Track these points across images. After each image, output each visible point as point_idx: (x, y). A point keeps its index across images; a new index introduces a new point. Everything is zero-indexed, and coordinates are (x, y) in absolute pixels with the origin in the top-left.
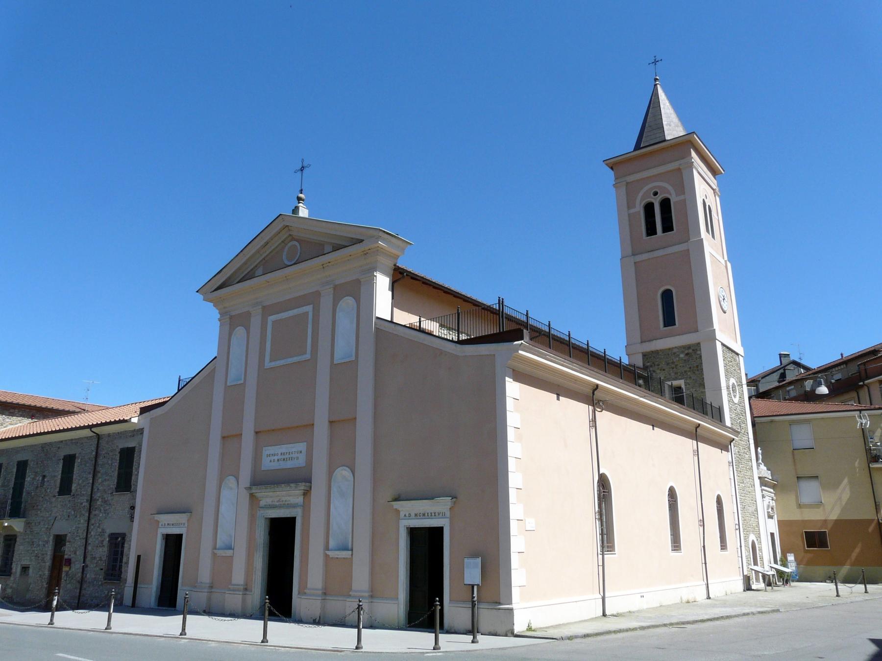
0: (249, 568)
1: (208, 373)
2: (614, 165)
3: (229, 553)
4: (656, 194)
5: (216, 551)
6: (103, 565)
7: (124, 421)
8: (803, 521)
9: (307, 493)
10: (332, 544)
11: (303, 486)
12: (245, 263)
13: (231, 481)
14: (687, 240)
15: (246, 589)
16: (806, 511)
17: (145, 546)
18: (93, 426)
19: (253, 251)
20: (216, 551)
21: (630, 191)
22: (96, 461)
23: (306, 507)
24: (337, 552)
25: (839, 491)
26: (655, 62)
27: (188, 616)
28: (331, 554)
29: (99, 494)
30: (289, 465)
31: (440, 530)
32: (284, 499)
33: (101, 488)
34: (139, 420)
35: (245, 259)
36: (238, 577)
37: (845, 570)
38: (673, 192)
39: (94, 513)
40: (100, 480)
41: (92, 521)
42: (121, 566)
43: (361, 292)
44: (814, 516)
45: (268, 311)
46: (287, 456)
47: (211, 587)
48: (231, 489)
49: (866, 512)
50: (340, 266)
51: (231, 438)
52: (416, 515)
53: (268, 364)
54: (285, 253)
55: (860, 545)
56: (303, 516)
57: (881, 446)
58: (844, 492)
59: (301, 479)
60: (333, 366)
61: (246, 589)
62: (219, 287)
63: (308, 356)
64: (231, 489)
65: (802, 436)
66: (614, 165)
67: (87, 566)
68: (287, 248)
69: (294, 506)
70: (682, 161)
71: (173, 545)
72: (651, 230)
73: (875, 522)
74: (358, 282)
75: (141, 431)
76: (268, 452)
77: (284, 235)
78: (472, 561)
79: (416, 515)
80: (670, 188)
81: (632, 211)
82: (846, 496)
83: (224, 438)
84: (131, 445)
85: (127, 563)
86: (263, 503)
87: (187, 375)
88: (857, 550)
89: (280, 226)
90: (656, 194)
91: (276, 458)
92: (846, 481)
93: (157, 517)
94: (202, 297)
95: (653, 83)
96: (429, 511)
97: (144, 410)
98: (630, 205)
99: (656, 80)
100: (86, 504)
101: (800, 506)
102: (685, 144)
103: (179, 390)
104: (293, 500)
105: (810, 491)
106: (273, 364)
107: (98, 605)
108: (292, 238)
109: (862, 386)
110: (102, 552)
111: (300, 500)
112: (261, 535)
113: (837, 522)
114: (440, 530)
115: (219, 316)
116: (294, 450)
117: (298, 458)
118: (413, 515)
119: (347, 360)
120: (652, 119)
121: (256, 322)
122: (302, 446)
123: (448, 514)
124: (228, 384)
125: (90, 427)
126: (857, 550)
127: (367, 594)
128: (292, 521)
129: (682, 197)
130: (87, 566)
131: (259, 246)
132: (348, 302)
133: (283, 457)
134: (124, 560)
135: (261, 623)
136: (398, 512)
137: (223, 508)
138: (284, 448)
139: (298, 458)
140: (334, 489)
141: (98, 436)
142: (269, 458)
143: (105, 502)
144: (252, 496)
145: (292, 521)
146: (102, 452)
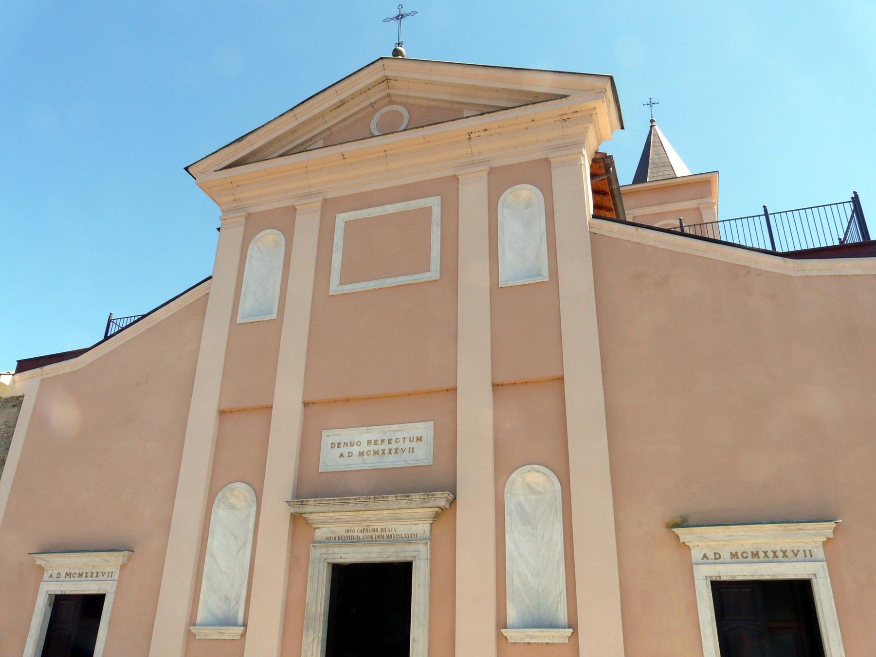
1: (194, 300)
3: (234, 632)
9: (445, 515)
10: (512, 614)
11: (441, 500)
12: (293, 131)
13: (239, 494)
26: (651, 104)
30: (390, 462)
32: (379, 526)
34: (13, 382)
35: (294, 124)
45: (330, 207)
46: (385, 446)
48: (233, 507)
50: (506, 139)
51: (247, 413)
52: (734, 555)
53: (335, 287)
59: (435, 485)
60: (495, 290)
63: (434, 274)
64: (233, 507)
68: (378, 115)
69: (410, 539)
75: (17, 402)
77: (377, 94)
83: (222, 413)
87: (125, 311)
89: (379, 76)
95: (650, 124)
97: (24, 366)
99: (652, 121)
103: (107, 338)
104: (402, 529)
106: (349, 288)
108: (390, 99)
111: (423, 528)
115: (220, 214)
116: (400, 435)
117: (411, 450)
119: (531, 281)
121: (307, 226)
122: (424, 429)
123: (820, 553)
124: (239, 321)
131: (327, 105)
133: (373, 448)
137: (215, 543)
138: (375, 433)
142: (337, 451)
144: (296, 519)
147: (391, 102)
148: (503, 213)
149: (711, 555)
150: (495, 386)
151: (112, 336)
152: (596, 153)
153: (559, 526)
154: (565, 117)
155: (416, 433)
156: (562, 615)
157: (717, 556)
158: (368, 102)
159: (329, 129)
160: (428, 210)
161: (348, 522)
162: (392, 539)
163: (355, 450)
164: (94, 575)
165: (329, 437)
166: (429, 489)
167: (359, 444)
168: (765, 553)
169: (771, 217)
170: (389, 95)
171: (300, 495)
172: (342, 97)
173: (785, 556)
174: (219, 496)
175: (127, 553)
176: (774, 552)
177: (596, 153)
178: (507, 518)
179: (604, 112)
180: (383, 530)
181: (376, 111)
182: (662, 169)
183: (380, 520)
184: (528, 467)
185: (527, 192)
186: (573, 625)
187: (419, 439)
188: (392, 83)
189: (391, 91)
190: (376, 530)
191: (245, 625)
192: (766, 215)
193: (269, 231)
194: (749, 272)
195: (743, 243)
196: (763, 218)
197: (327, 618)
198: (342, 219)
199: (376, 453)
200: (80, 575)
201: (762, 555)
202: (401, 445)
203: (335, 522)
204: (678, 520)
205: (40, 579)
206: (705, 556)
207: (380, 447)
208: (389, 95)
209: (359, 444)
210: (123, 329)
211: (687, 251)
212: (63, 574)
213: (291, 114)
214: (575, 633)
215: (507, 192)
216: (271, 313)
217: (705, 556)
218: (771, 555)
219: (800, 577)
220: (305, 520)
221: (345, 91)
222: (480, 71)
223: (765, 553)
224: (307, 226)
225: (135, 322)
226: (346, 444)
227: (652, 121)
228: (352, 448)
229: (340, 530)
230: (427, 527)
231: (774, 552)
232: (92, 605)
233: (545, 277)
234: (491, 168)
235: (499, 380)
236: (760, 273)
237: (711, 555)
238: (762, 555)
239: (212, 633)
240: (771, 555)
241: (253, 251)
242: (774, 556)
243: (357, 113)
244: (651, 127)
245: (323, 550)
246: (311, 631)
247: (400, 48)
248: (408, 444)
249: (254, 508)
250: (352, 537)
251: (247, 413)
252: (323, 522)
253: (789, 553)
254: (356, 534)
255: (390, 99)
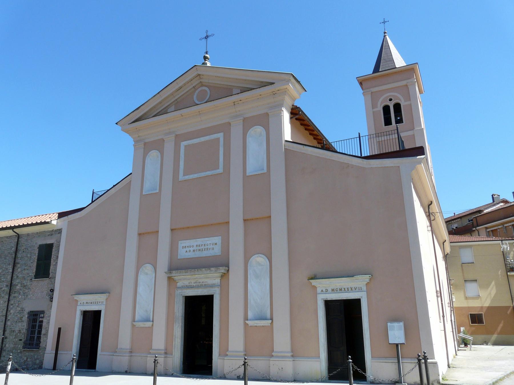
0: (168, 336)
1: (124, 186)
2: (362, 82)
3: (149, 324)
4: (391, 100)
5: (134, 323)
6: (23, 337)
7: (45, 223)
8: (468, 307)
9: (225, 276)
10: (250, 315)
11: (222, 270)
12: (160, 103)
13: (148, 268)
14: (413, 129)
15: (166, 353)
16: (470, 301)
17: (63, 320)
18: (15, 227)
19: (169, 93)
20: (134, 323)
21: (374, 98)
22: (16, 254)
23: (224, 286)
24: (256, 322)
25: (490, 289)
26: (384, 22)
27: (158, 378)
28: (250, 323)
29: (18, 281)
30: (204, 254)
31: (357, 302)
32: (201, 281)
33: (20, 276)
34: (57, 223)
36: (159, 342)
37: (494, 337)
38: (402, 99)
39: (13, 295)
40: (19, 270)
41: (12, 302)
42: (39, 338)
43: (267, 121)
44: (476, 304)
45: (179, 138)
46: (203, 247)
47: (131, 352)
48: (147, 274)
49: (506, 302)
50: (251, 103)
51: (148, 235)
52: (333, 290)
53: (181, 177)
54: (196, 94)
55: (502, 322)
56: (221, 294)
57: (513, 262)
58: (492, 290)
59: (221, 264)
60: (246, 178)
61: (167, 353)
62: (138, 119)
63: (220, 170)
64: (147, 274)
65: (467, 256)
66: (362, 82)
67: (6, 338)
68: (197, 92)
69: (212, 286)
70: (409, 80)
71: (92, 321)
72: (388, 122)
73: (511, 308)
74: (267, 115)
75: (59, 231)
76: (184, 245)
77: (195, 83)
78: (396, 324)
79: (333, 290)
80: (400, 96)
81: (375, 110)
82: (494, 292)
84: (49, 242)
85: (46, 335)
86: (179, 284)
88: (501, 325)
89: (195, 74)
90: (391, 100)
91: (192, 249)
92: (493, 283)
93: (77, 297)
94: (120, 128)
95: (383, 35)
96: (353, 287)
97: (61, 215)
98: (374, 106)
99: (385, 33)
100: (7, 289)
101: (466, 298)
102: (409, 71)
103: (93, 202)
104: (210, 282)
105: (472, 289)
106: (187, 177)
107: (35, 369)
108: (202, 84)
109: (474, 230)
110: (23, 326)
111: (217, 281)
112: (179, 309)
113: (489, 308)
114: (357, 302)
116: (208, 242)
117: (213, 249)
118: (330, 290)
119: (260, 172)
120: (382, 56)
121: (169, 147)
122: (217, 240)
123: (364, 288)
125: (11, 228)
126: (501, 325)
127: (289, 354)
128: (209, 300)
129: (408, 103)
130: (6, 338)
132: (258, 130)
133: (198, 248)
134: (43, 332)
135: (152, 378)
136: (315, 288)
137: (140, 289)
138: (199, 241)
139: (213, 249)
140: (250, 272)
141: (18, 236)
142: (185, 250)
143: (25, 286)
144: (170, 279)
145: (209, 300)
146: (21, 248)
147: (202, 85)
148: (249, 139)
149: (324, 290)
150: (245, 220)
151: (95, 201)
152: (293, 105)
153: (268, 280)
154: (274, 93)
155: (214, 242)
156: (269, 316)
157: (327, 290)
158: (192, 87)
159: (176, 100)
160: (218, 139)
161: (189, 279)
162: (206, 286)
163: (192, 249)
164: (96, 303)
165: (182, 244)
166: (217, 266)
167: (193, 246)
168: (344, 289)
169: (361, 138)
170: (201, 82)
171: (171, 269)
172: (180, 85)
173: (352, 290)
174: (141, 270)
175: (107, 294)
176: (348, 288)
177: (293, 105)
178: (249, 276)
179: (292, 87)
180: (203, 282)
181: (196, 90)
182: (388, 63)
183: (200, 278)
184: (257, 255)
185: (259, 129)
186: (272, 319)
187: (216, 244)
188: (201, 77)
189: (201, 80)
190: (200, 282)
191: (153, 321)
192: (359, 137)
193: (154, 151)
194: (348, 166)
195: (346, 153)
196: (358, 139)
197: (183, 318)
198: (183, 144)
199: (199, 250)
200: (91, 303)
201: (343, 289)
202: (209, 247)
203: (184, 279)
204: (313, 276)
205: (77, 305)
206: (322, 291)
207: (201, 248)
208: (201, 82)
209: (193, 246)
210: (101, 196)
211: (323, 157)
212: (85, 303)
213: (159, 95)
214: (272, 322)
215: (250, 130)
216: (156, 190)
217: (322, 291)
218: (346, 289)
219: (356, 298)
220: (173, 279)
221: (181, 83)
222: (237, 72)
223: (344, 289)
224: (169, 147)
225: (105, 193)
226: (188, 247)
227: (385, 33)
228: (189, 248)
229: (186, 283)
230: (219, 281)
231: (348, 288)
232: (97, 314)
233: (265, 171)
234: (245, 118)
235: (246, 218)
236: (353, 166)
237: (324, 290)
238: (343, 289)
239: (141, 324)
240: (346, 289)
241: (148, 161)
242: (347, 290)
243: (187, 92)
244: (385, 36)
245: (180, 291)
246: (177, 323)
247: (207, 55)
248: (211, 246)
249: (154, 274)
250: (191, 286)
251: (148, 235)
252: (181, 280)
253: (353, 289)
254: (192, 284)
255: (202, 84)
